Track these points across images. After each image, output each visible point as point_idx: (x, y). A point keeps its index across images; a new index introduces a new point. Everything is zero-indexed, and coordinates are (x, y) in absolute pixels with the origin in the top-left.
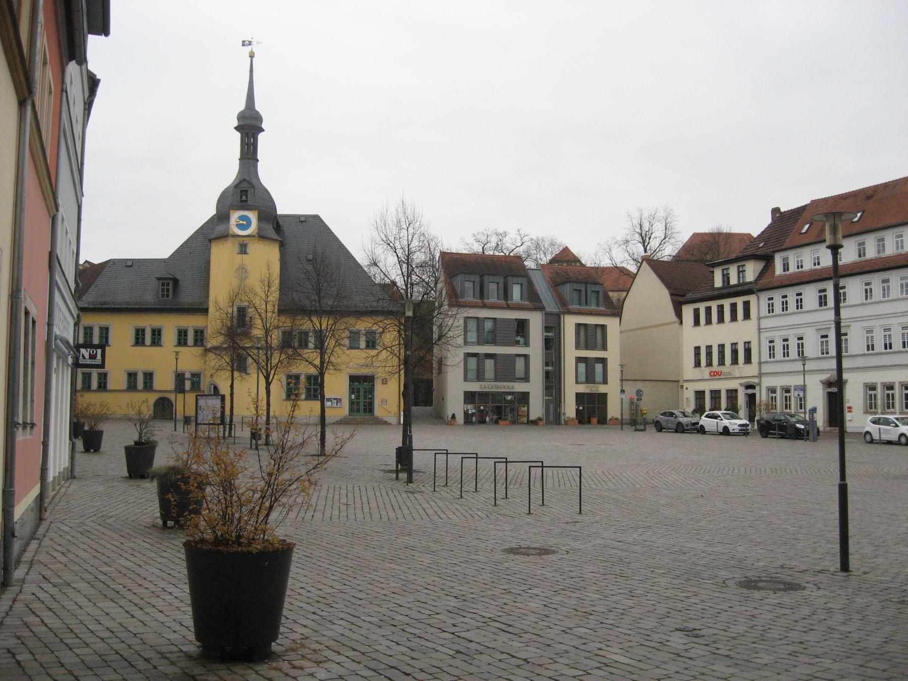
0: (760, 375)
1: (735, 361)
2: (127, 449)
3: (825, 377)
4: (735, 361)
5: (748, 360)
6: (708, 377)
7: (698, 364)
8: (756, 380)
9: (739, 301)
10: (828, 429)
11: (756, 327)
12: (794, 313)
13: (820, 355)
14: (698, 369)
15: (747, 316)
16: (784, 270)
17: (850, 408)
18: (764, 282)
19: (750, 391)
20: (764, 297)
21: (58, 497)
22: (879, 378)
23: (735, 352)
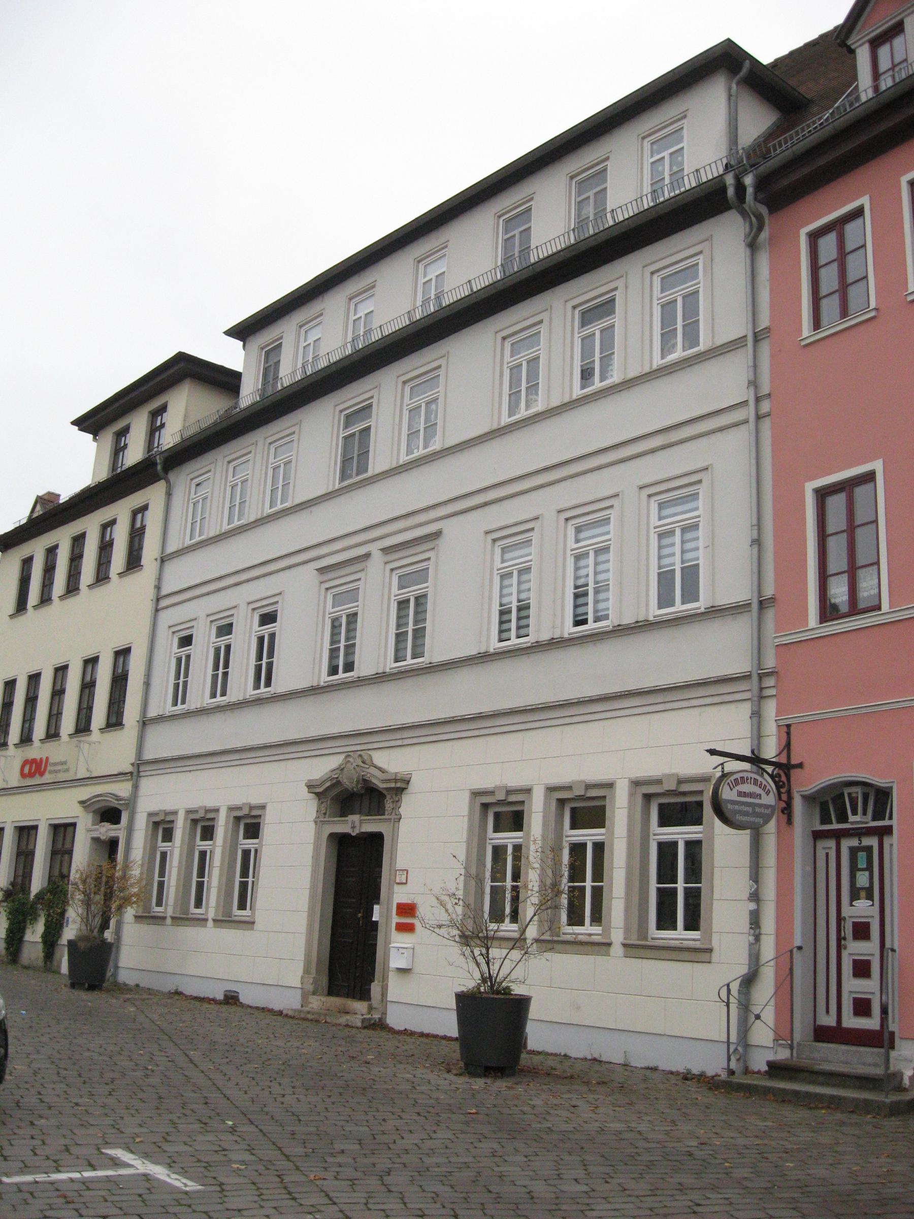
0: (139, 769)
2: (462, 998)
3: (322, 767)
6: (14, 780)
8: (123, 789)
10: (317, 1003)
13: (324, 678)
17: (407, 910)
21: (361, 1182)
22: (539, 763)
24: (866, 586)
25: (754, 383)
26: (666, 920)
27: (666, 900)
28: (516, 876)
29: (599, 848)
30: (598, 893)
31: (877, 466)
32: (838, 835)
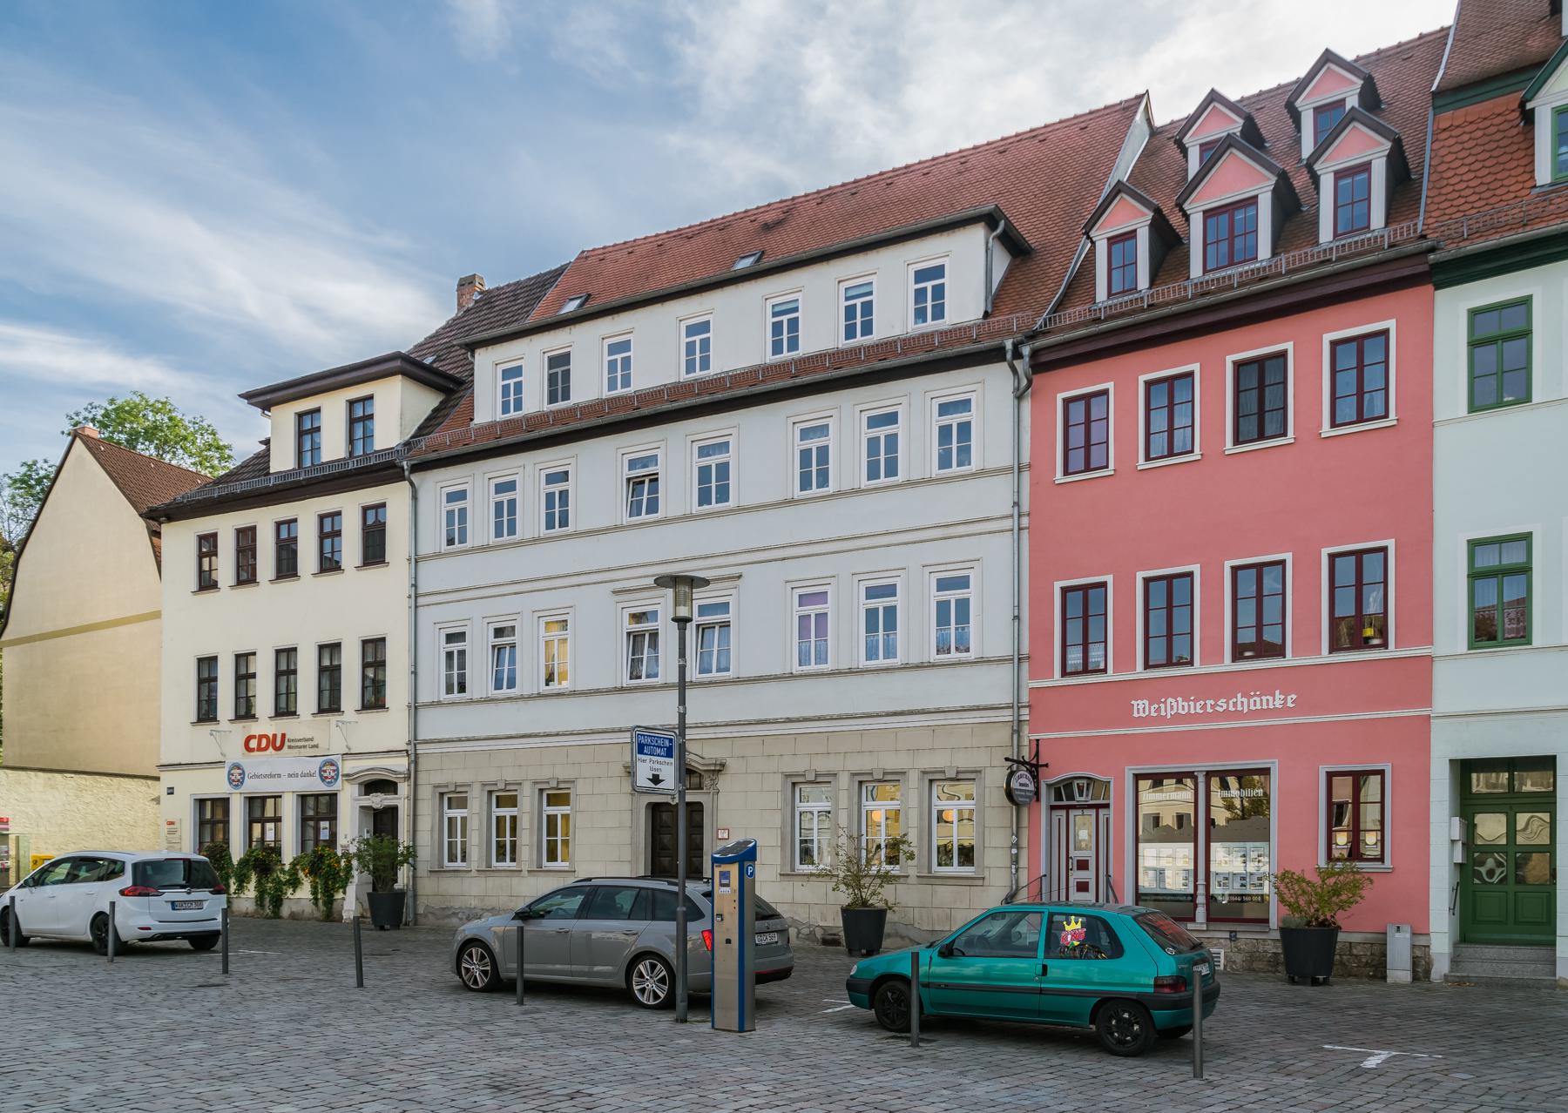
1: (330, 703)
4: (330, 703)
5: (374, 699)
7: (206, 712)
8: (401, 764)
9: (350, 505)
11: (406, 589)
12: (536, 541)
14: (207, 728)
15: (374, 552)
16: (552, 399)
18: (443, 437)
19: (378, 800)
20: (435, 485)
23: (330, 674)
24: (1096, 654)
25: (1017, 504)
26: (501, 856)
27: (501, 847)
28: (464, 835)
29: (514, 819)
30: (513, 844)
31: (1109, 579)
32: (1068, 808)
